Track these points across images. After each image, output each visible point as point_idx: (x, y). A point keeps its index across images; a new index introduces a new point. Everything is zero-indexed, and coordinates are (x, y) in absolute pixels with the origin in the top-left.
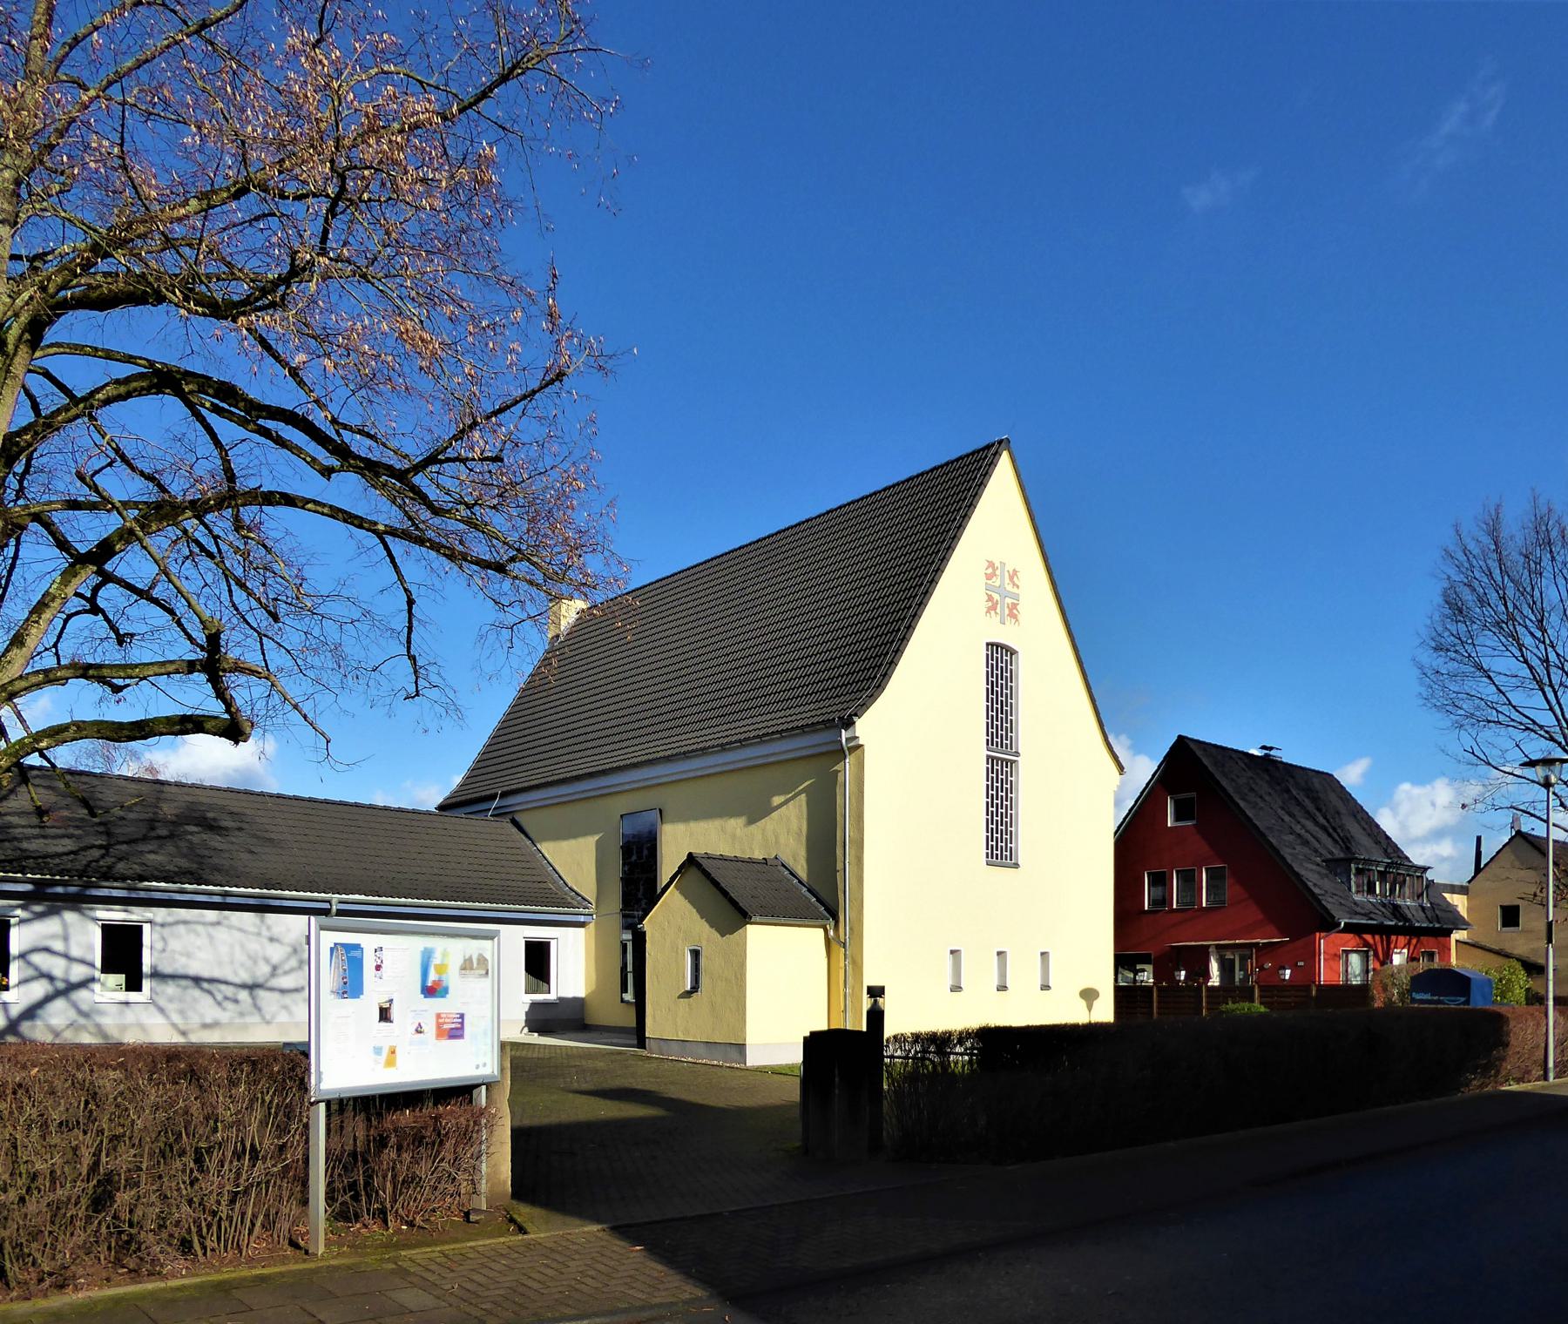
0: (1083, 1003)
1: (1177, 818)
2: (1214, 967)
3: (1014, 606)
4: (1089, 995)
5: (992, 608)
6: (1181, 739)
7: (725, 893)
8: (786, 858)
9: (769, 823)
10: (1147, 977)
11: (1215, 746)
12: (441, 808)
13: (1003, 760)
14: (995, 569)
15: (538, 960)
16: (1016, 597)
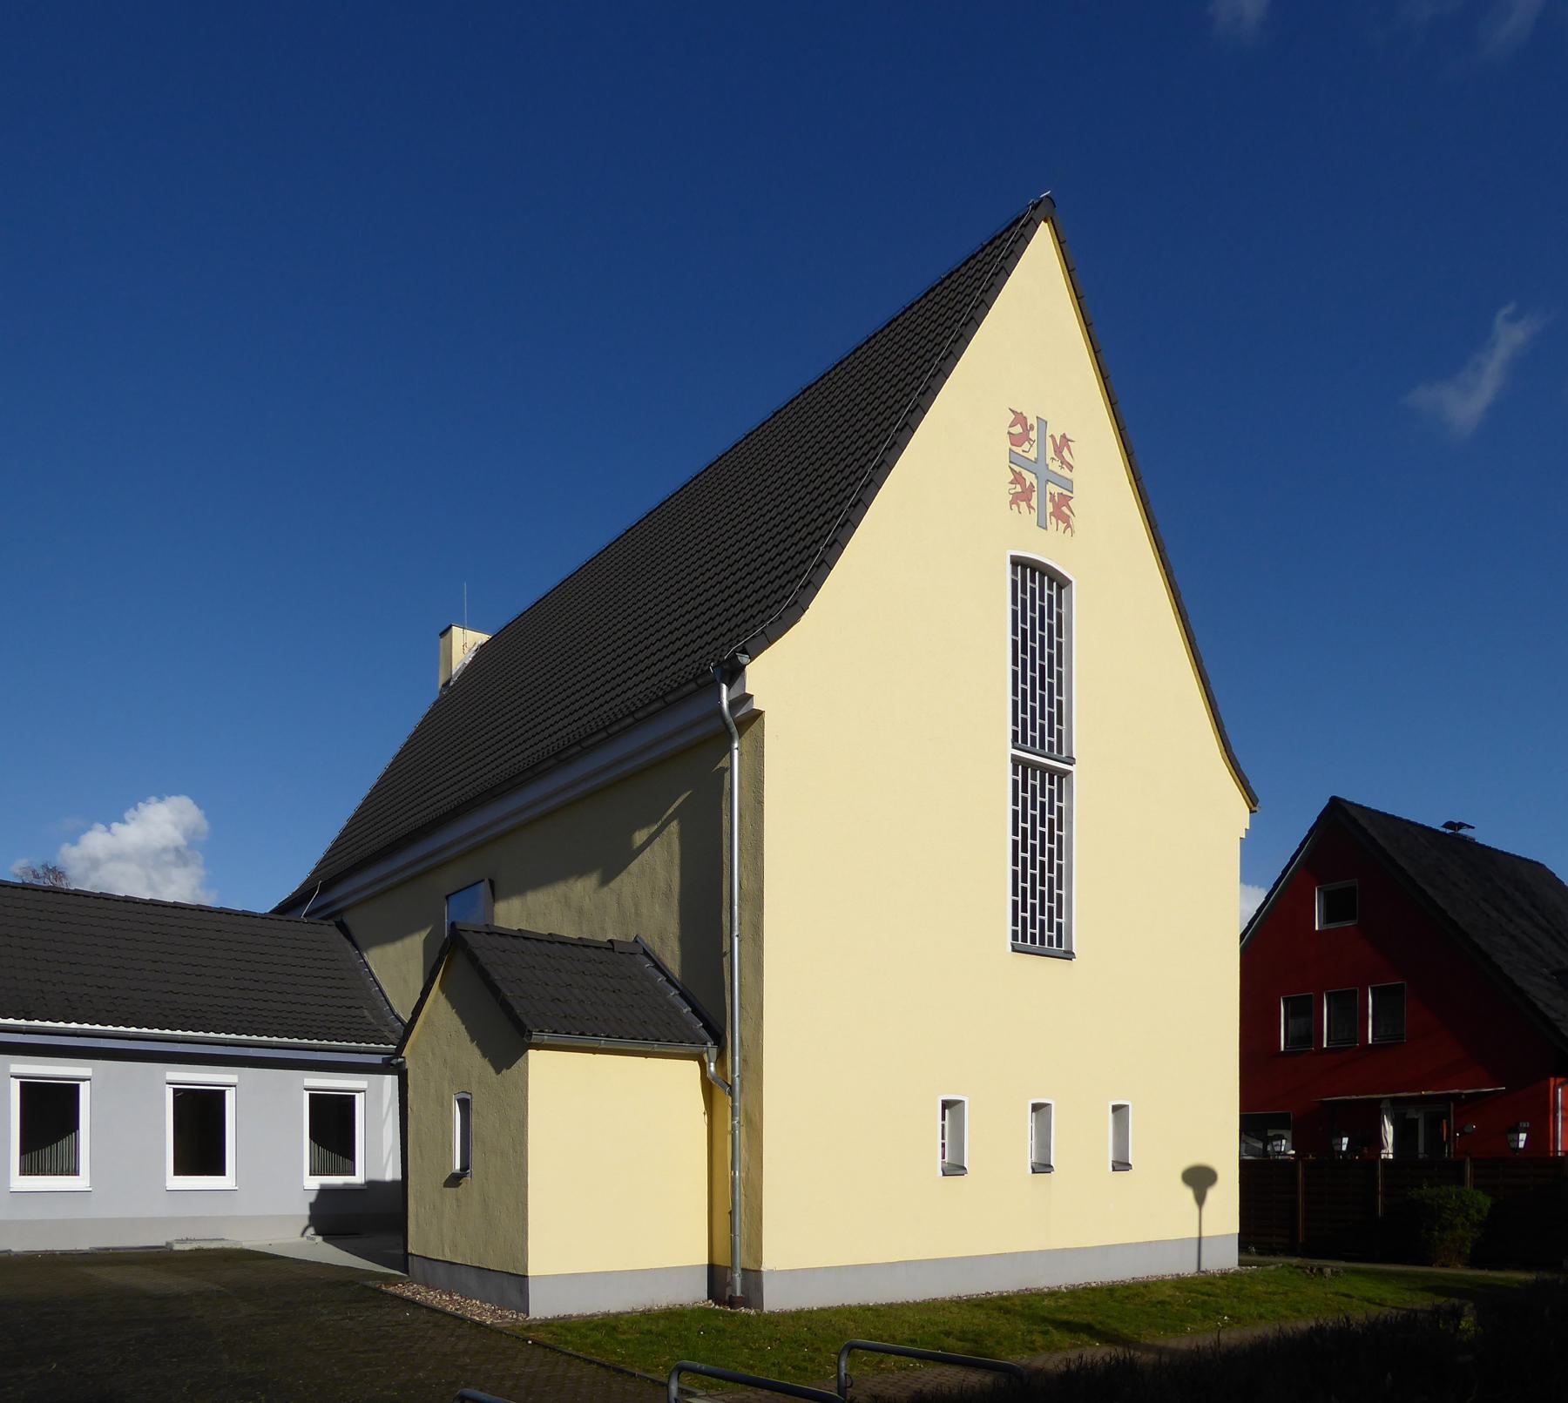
0: (1188, 1194)
1: (1329, 917)
2: (1389, 1130)
3: (1064, 500)
4: (1200, 1179)
5: (1022, 496)
6: (1335, 803)
7: (495, 990)
8: (652, 941)
9: (625, 882)
10: (1285, 1147)
11: (1385, 815)
12: (277, 911)
13: (1044, 769)
14: (1027, 429)
15: (332, 1126)
16: (1068, 485)
